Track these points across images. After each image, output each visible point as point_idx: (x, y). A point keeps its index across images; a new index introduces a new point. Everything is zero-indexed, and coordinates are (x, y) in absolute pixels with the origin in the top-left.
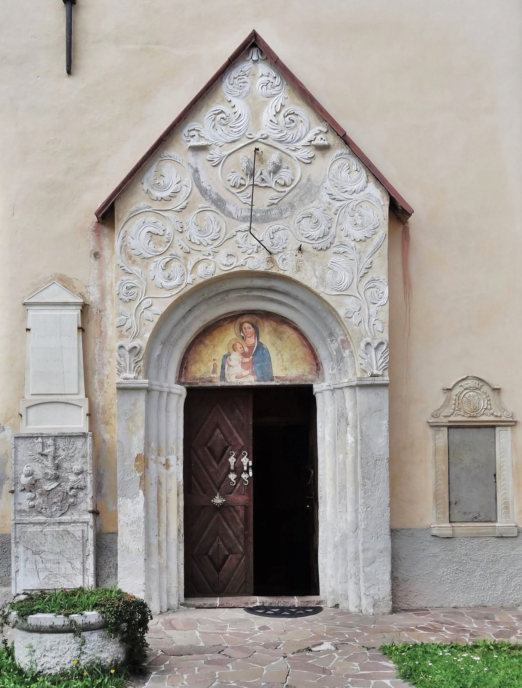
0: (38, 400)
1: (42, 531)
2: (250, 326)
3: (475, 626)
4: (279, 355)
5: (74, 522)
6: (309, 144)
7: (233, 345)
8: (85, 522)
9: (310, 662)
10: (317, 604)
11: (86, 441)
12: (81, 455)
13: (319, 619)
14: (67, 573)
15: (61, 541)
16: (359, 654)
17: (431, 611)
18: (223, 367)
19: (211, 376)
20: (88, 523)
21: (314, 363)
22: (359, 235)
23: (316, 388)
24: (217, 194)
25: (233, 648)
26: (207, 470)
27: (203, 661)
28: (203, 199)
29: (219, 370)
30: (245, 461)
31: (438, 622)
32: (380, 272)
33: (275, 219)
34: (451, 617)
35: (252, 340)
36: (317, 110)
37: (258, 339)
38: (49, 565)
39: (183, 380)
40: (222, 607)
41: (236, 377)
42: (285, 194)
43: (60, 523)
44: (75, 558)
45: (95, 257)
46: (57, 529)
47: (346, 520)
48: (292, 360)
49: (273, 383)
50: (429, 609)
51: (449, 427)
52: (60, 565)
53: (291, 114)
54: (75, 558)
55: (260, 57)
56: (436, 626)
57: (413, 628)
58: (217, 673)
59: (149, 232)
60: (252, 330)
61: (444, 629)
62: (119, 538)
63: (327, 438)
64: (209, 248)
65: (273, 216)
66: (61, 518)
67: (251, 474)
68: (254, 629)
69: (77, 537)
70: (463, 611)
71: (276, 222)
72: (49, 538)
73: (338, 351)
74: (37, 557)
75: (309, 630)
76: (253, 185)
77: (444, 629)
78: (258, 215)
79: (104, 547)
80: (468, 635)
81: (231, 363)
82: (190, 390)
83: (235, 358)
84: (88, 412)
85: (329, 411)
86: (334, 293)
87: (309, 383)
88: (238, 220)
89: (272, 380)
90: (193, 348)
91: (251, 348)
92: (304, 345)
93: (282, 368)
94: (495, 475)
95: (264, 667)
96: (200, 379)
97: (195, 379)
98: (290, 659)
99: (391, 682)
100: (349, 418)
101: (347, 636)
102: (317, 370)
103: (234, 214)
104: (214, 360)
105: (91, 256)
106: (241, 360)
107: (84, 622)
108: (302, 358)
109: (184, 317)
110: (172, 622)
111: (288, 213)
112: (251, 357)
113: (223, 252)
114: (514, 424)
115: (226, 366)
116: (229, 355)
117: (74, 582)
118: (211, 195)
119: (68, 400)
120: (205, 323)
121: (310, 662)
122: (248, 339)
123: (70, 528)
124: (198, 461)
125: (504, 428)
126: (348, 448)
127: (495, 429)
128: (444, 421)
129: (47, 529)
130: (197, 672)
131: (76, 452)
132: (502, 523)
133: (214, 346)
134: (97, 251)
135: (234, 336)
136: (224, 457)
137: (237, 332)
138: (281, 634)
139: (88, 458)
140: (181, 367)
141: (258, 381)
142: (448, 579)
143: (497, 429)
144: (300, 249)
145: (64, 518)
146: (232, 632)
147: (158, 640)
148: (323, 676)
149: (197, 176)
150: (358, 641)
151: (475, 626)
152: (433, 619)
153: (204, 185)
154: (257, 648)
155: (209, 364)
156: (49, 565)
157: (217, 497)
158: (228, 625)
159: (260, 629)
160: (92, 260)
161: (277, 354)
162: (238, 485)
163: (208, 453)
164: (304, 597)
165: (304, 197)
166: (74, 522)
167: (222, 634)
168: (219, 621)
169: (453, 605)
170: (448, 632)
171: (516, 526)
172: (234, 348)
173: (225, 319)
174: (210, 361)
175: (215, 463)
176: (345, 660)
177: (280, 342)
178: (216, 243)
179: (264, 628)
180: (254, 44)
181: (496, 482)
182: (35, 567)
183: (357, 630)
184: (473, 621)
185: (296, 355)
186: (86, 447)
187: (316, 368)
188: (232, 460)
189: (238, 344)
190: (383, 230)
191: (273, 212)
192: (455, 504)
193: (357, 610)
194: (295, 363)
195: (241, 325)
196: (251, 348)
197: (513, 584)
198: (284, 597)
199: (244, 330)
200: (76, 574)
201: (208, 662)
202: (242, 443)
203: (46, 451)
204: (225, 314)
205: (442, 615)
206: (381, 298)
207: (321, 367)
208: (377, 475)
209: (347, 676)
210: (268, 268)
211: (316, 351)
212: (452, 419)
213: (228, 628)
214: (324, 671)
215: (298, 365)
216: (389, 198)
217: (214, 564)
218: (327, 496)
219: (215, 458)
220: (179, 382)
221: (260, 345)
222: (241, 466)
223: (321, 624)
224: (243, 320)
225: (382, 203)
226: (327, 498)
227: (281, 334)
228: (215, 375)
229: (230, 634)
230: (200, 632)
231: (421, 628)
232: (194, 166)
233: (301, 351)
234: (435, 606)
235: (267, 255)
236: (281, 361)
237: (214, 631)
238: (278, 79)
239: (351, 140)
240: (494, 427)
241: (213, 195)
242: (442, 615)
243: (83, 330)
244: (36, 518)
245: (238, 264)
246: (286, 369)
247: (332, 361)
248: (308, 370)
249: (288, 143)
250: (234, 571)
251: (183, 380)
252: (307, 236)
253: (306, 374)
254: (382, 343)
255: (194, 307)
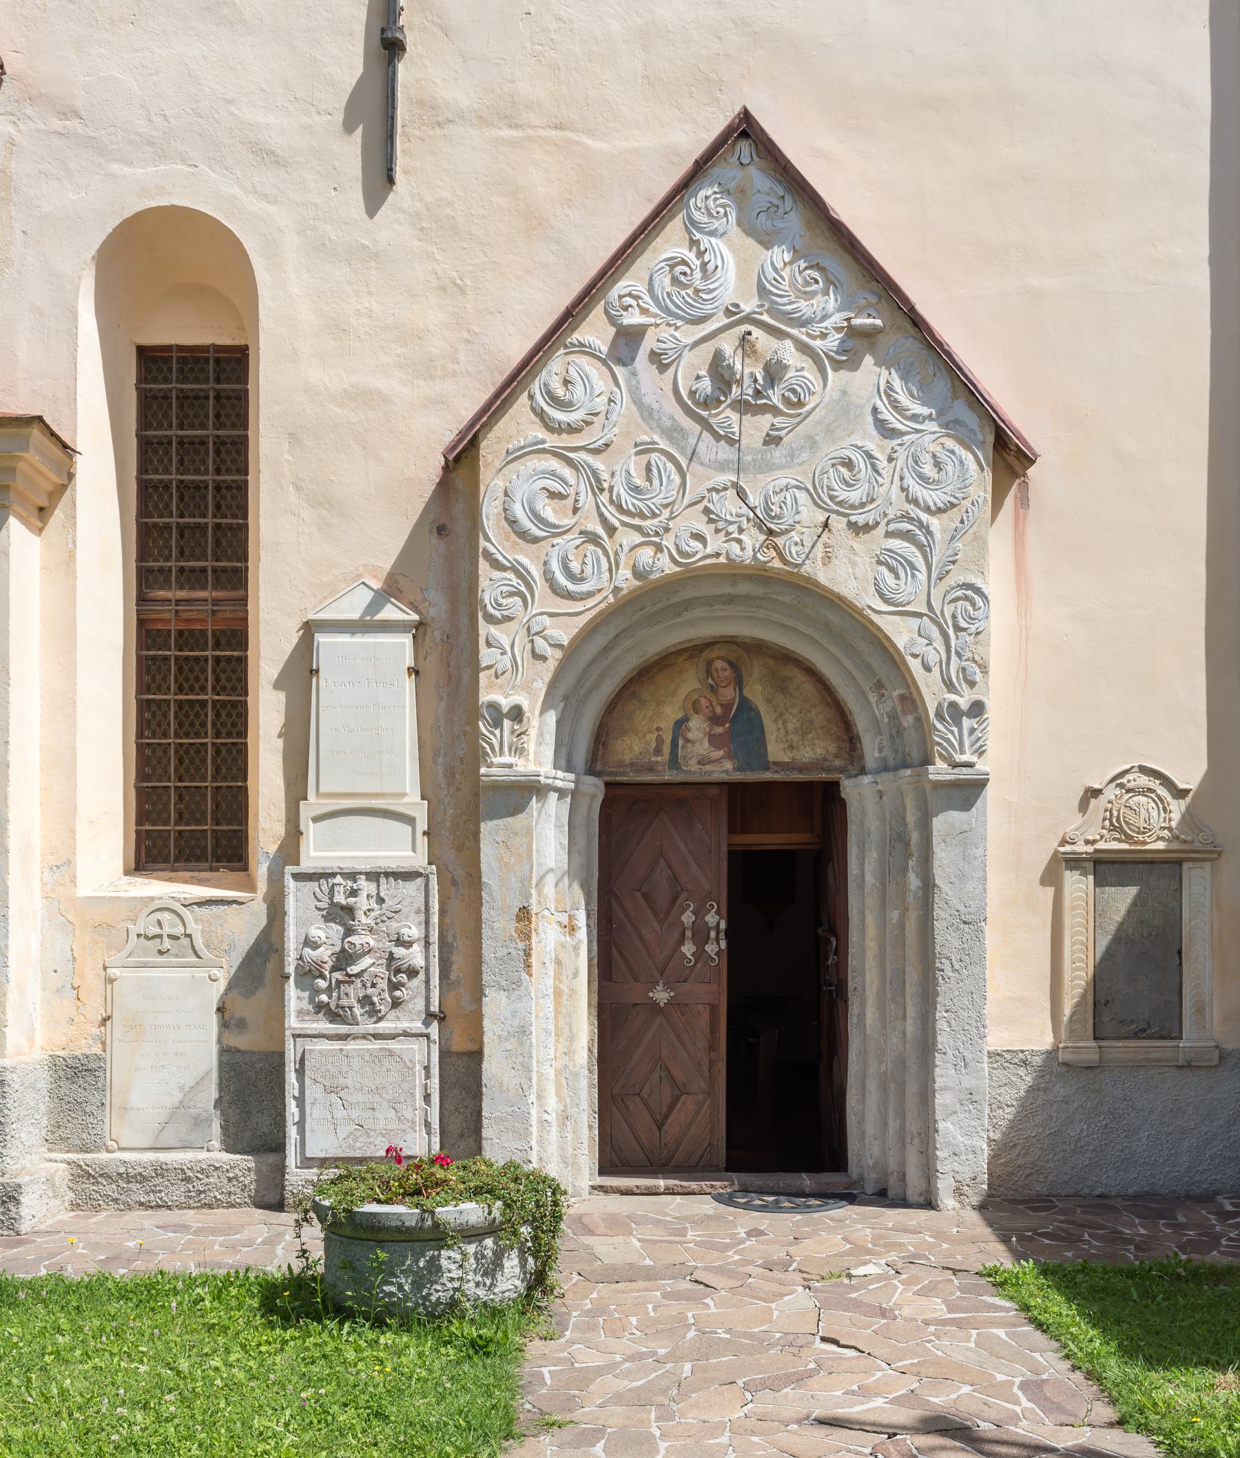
2: (725, 665)
3: (1143, 1232)
4: (780, 724)
7: (694, 703)
9: (854, 1295)
16: (939, 1282)
21: (846, 738)
25: (706, 1269)
26: (640, 936)
27: (658, 1294)
29: (667, 748)
30: (711, 919)
31: (1072, 1223)
33: (780, 467)
35: (729, 693)
38: (355, 1114)
39: (599, 766)
40: (669, 1192)
41: (699, 763)
42: (798, 419)
43: (377, 1036)
45: (439, 533)
47: (904, 1034)
48: (805, 730)
49: (768, 776)
52: (376, 1113)
58: (690, 1315)
60: (729, 673)
63: (870, 879)
64: (655, 521)
65: (777, 461)
70: (1118, 1203)
72: (356, 1063)
73: (893, 716)
77: (1086, 1237)
78: (749, 458)
79: (462, 1078)
80: (1132, 1247)
81: (689, 736)
83: (697, 727)
89: (766, 767)
91: (727, 707)
92: (828, 704)
93: (786, 745)
94: (1180, 952)
95: (773, 1305)
96: (632, 764)
97: (621, 764)
98: (816, 1290)
99: (1007, 1334)
104: (658, 729)
105: (430, 532)
108: (822, 727)
109: (606, 650)
110: (584, 1219)
114: (1215, 856)
118: (660, 419)
121: (854, 1295)
122: (721, 691)
124: (626, 921)
125: (1198, 864)
126: (910, 898)
129: (351, 1046)
130: (652, 1314)
132: (1190, 1040)
133: (659, 703)
134: (442, 521)
135: (696, 685)
138: (790, 1245)
142: (1089, 1144)
148: (884, 1321)
149: (634, 383)
151: (1143, 1232)
152: (1063, 1218)
153: (648, 400)
154: (750, 1269)
159: (749, 1234)
160: (434, 539)
161: (776, 721)
162: (699, 965)
163: (642, 901)
164: (819, 1175)
165: (835, 425)
167: (681, 1243)
169: (1098, 1191)
171: (1217, 1047)
172: (696, 708)
173: (680, 652)
174: (650, 732)
175: (656, 925)
176: (917, 1293)
177: (782, 697)
179: (755, 1233)
181: (1181, 964)
182: (329, 1117)
184: (1137, 1221)
185: (811, 722)
189: (703, 700)
194: (810, 736)
196: (727, 707)
197: (1208, 1154)
198: (783, 1175)
199: (715, 674)
201: (666, 1296)
202: (707, 886)
209: (927, 1323)
212: (1101, 845)
213: (690, 1233)
214: (883, 1313)
217: (651, 1113)
218: (867, 986)
219: (655, 914)
221: (745, 703)
226: (868, 992)
228: (659, 759)
230: (639, 1240)
236: (782, 733)
241: (664, 419)
243: (417, 673)
246: (792, 747)
247: (880, 733)
248: (832, 749)
255: (625, 630)
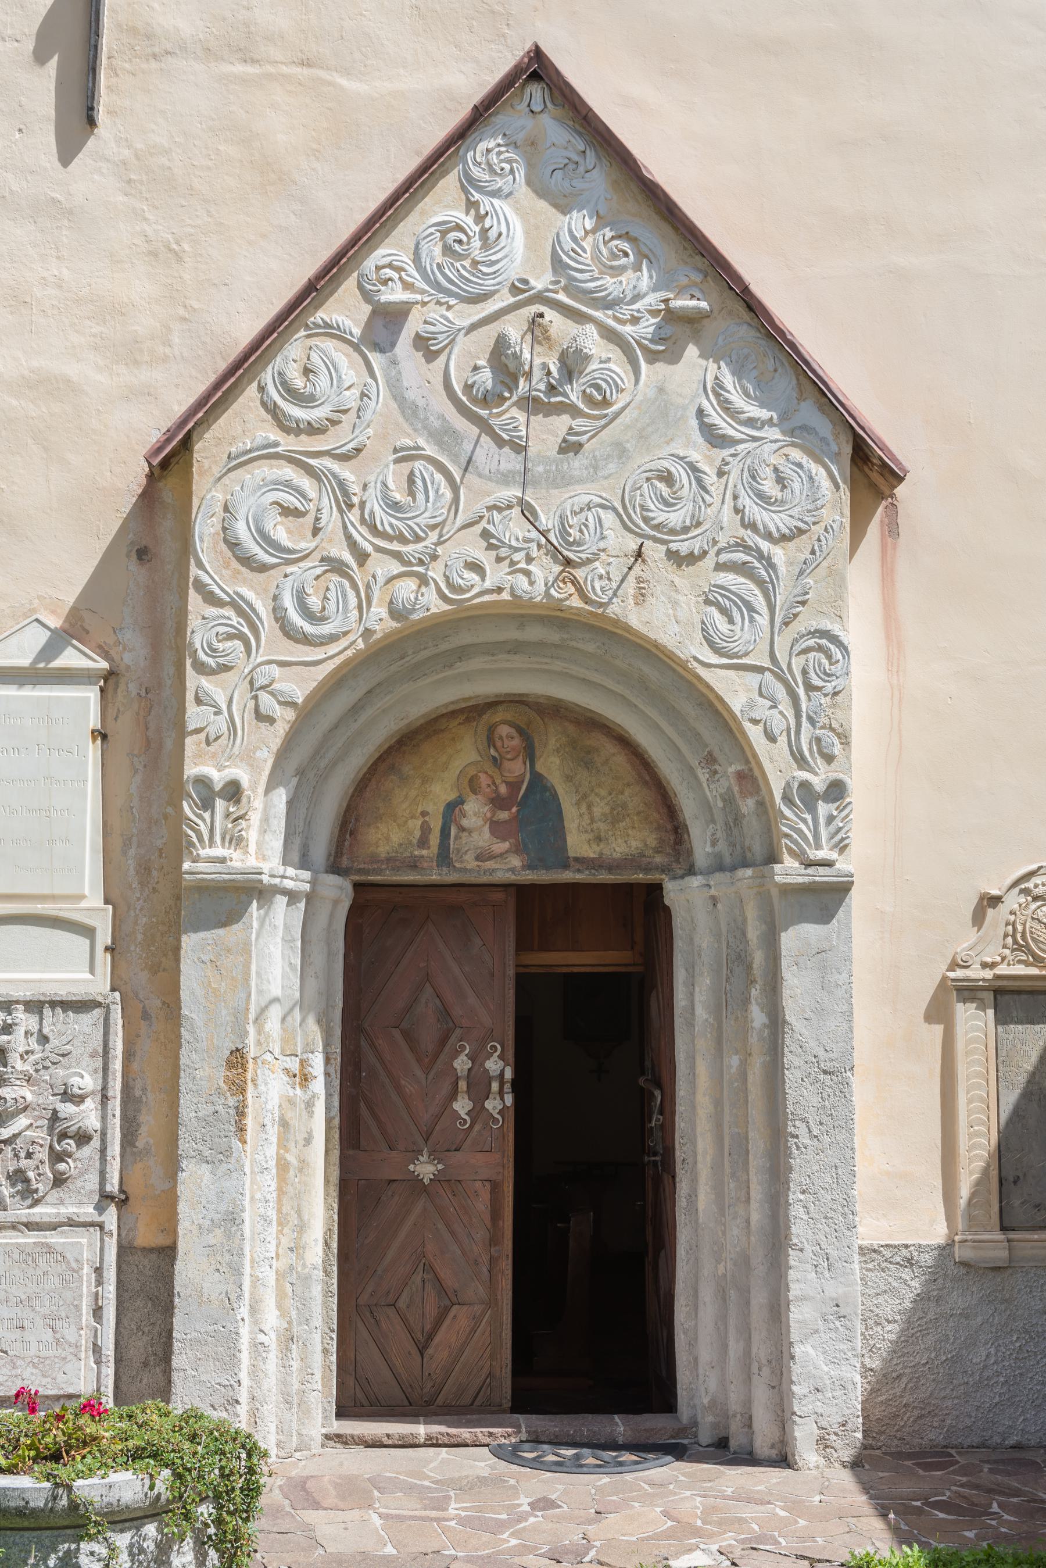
7: (471, 781)
13: (682, 1478)
14: (42, 1354)
15: (31, 1271)
17: (958, 1458)
18: (445, 833)
19: (416, 853)
23: (674, 893)
26: (398, 1088)
29: (434, 839)
30: (493, 1065)
31: (977, 1487)
33: (580, 481)
34: (1008, 1474)
35: (517, 768)
36: (682, 230)
39: (345, 862)
40: (432, 1443)
42: (603, 422)
43: (31, 1226)
44: (63, 1315)
50: (953, 1452)
52: (26, 1333)
54: (63, 1315)
56: (975, 1500)
57: (918, 1503)
60: (517, 742)
61: (995, 1508)
65: (576, 473)
66: (31, 1211)
67: (509, 1100)
69: (72, 1261)
75: (658, 1510)
77: (995, 1508)
78: (540, 469)
81: (465, 823)
85: (704, 945)
89: (566, 866)
90: (373, 782)
91: (514, 786)
92: (646, 783)
93: (591, 836)
96: (388, 860)
97: (374, 859)
100: (755, 966)
101: (756, 1527)
102: (676, 843)
104: (424, 814)
105: (128, 556)
106: (489, 815)
107: (105, 1500)
111: (611, 466)
112: (514, 809)
115: (453, 831)
116: (460, 801)
120: (403, 724)
122: (507, 765)
126: (754, 1039)
133: (426, 780)
134: (144, 543)
135: (474, 757)
136: (442, 1057)
137: (481, 747)
140: (341, 830)
141: (530, 867)
142: (998, 1374)
146: (463, 1514)
147: (278, 1536)
149: (394, 373)
150: (784, 1543)
152: (964, 1479)
153: (411, 395)
155: (411, 823)
158: (452, 1493)
160: (133, 565)
161: (578, 804)
162: (477, 1127)
165: (650, 429)
167: (438, 1520)
168: (426, 1483)
169: (1012, 1440)
170: (1006, 1517)
172: (474, 786)
173: (453, 714)
174: (413, 817)
175: (419, 1072)
179: (543, 1504)
180: (537, 70)
183: (778, 1510)
187: (672, 838)
192: (1015, 1182)
194: (622, 824)
196: (514, 786)
199: (499, 744)
200: (64, 1359)
204: (452, 703)
205: (986, 1468)
207: (686, 836)
211: (672, 796)
212: (1003, 970)
213: (453, 1505)
215: (630, 832)
216: (851, 439)
218: (699, 1158)
219: (419, 1060)
221: (538, 781)
223: (688, 1493)
225: (834, 448)
226: (700, 1165)
227: (589, 752)
228: (425, 852)
229: (461, 1521)
230: (381, 1516)
231: (937, 1505)
234: (968, 1442)
236: (587, 819)
237: (417, 1513)
238: (591, 155)
239: (760, 303)
241: (432, 418)
242: (986, 1468)
243: (104, 737)
246: (599, 839)
248: (652, 841)
250: (461, 1351)
253: (650, 852)
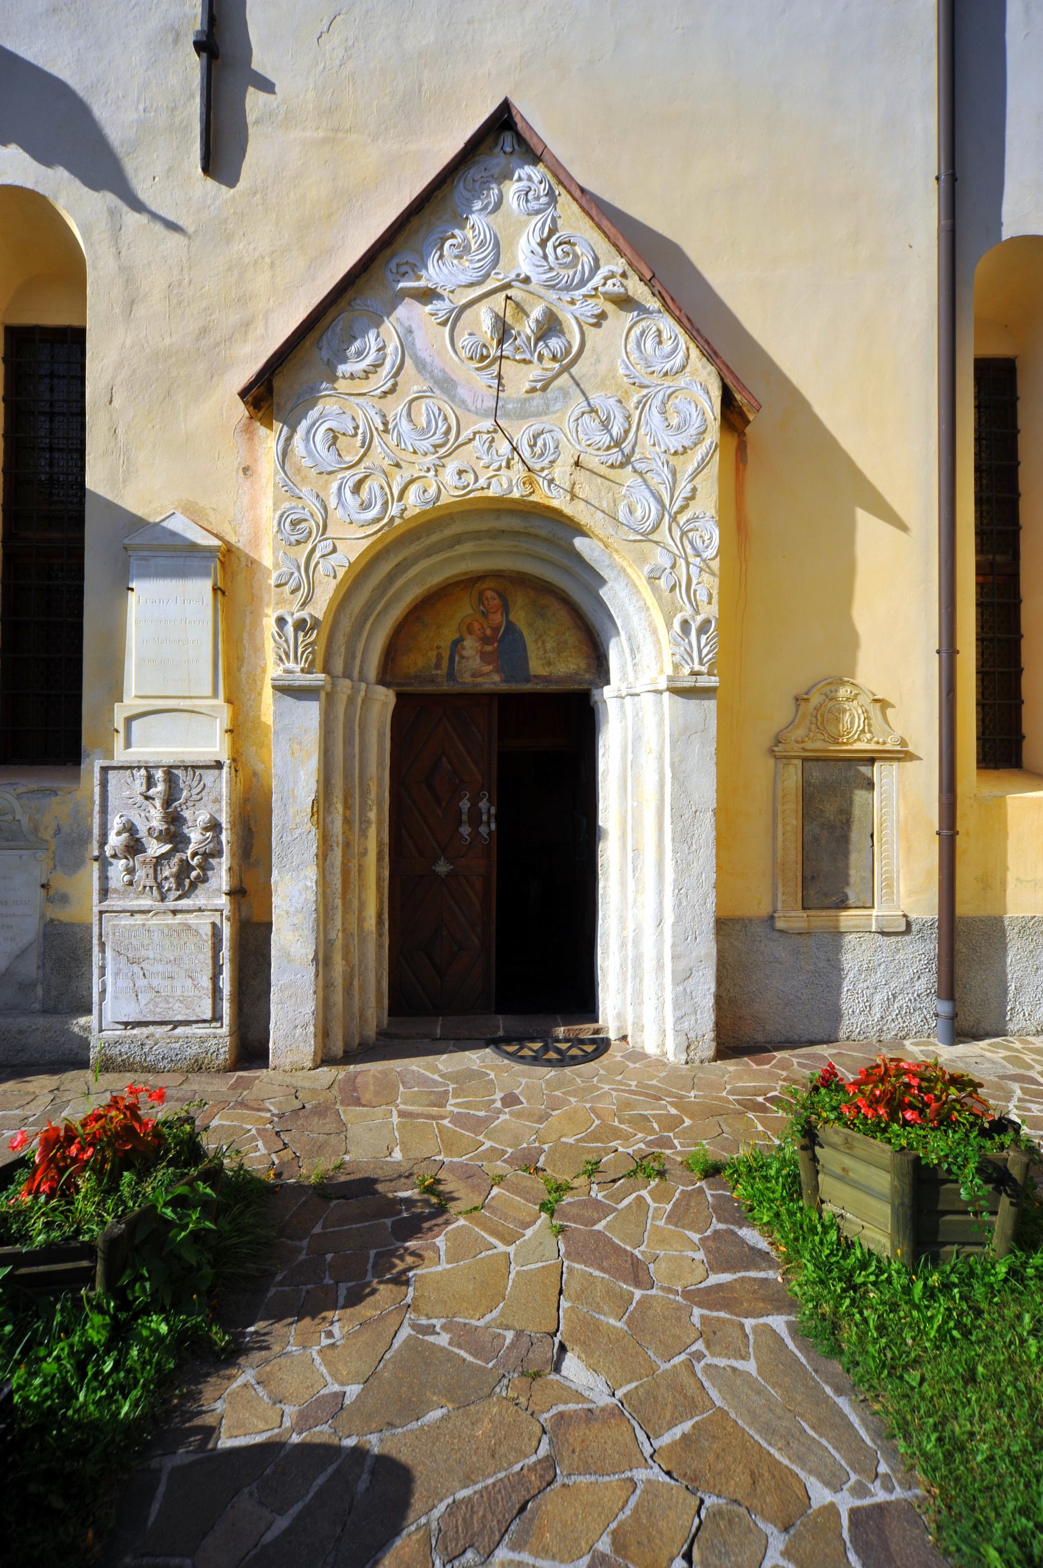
0: (149, 705)
1: (144, 925)
2: (495, 595)
4: (540, 644)
5: (200, 910)
6: (593, 293)
8: (216, 910)
10: (593, 1034)
11: (221, 774)
12: (211, 798)
20: (222, 911)
22: (674, 443)
24: (443, 371)
28: (421, 379)
29: (445, 663)
32: (707, 504)
35: (497, 618)
37: (507, 618)
43: (174, 912)
45: (245, 474)
46: (170, 922)
51: (805, 760)
53: (565, 243)
55: (516, 147)
59: (331, 429)
60: (497, 601)
62: (274, 937)
67: (493, 826)
68: (494, 1101)
71: (539, 419)
72: (156, 937)
74: (136, 968)
76: (501, 357)
81: (464, 653)
82: (402, 698)
83: (470, 645)
84: (229, 727)
86: (631, 538)
87: (586, 687)
88: (477, 413)
91: (495, 630)
96: (416, 677)
103: (470, 404)
104: (438, 647)
108: (575, 647)
111: (558, 404)
113: (452, 466)
115: (457, 658)
117: (197, 1010)
118: (432, 371)
119: (195, 706)
122: (491, 616)
123: (192, 919)
127: (873, 765)
128: (795, 750)
129: (154, 921)
131: (203, 793)
135: (470, 611)
139: (224, 803)
143: (877, 765)
144: (577, 464)
145: (185, 903)
156: (155, 983)
157: (442, 862)
161: (536, 641)
166: (200, 910)
168: (436, 1077)
172: (470, 630)
174: (431, 649)
178: (442, 451)
182: (132, 985)
185: (566, 642)
186: (222, 783)
188: (465, 805)
190: (713, 434)
191: (535, 403)
193: (658, 1051)
194: (565, 654)
195: (481, 593)
196: (495, 630)
199: (486, 602)
203: (151, 792)
206: (707, 547)
208: (696, 836)
210: (524, 493)
213: (452, 1101)
220: (382, 681)
221: (511, 627)
222: (478, 817)
224: (484, 586)
228: (439, 672)
232: (407, 324)
233: (572, 637)
235: (523, 473)
240: (872, 761)
244: (135, 902)
245: (478, 485)
246: (549, 664)
248: (583, 665)
249: (560, 289)
251: (388, 678)
252: (588, 442)
253: (581, 672)
254: (708, 622)
